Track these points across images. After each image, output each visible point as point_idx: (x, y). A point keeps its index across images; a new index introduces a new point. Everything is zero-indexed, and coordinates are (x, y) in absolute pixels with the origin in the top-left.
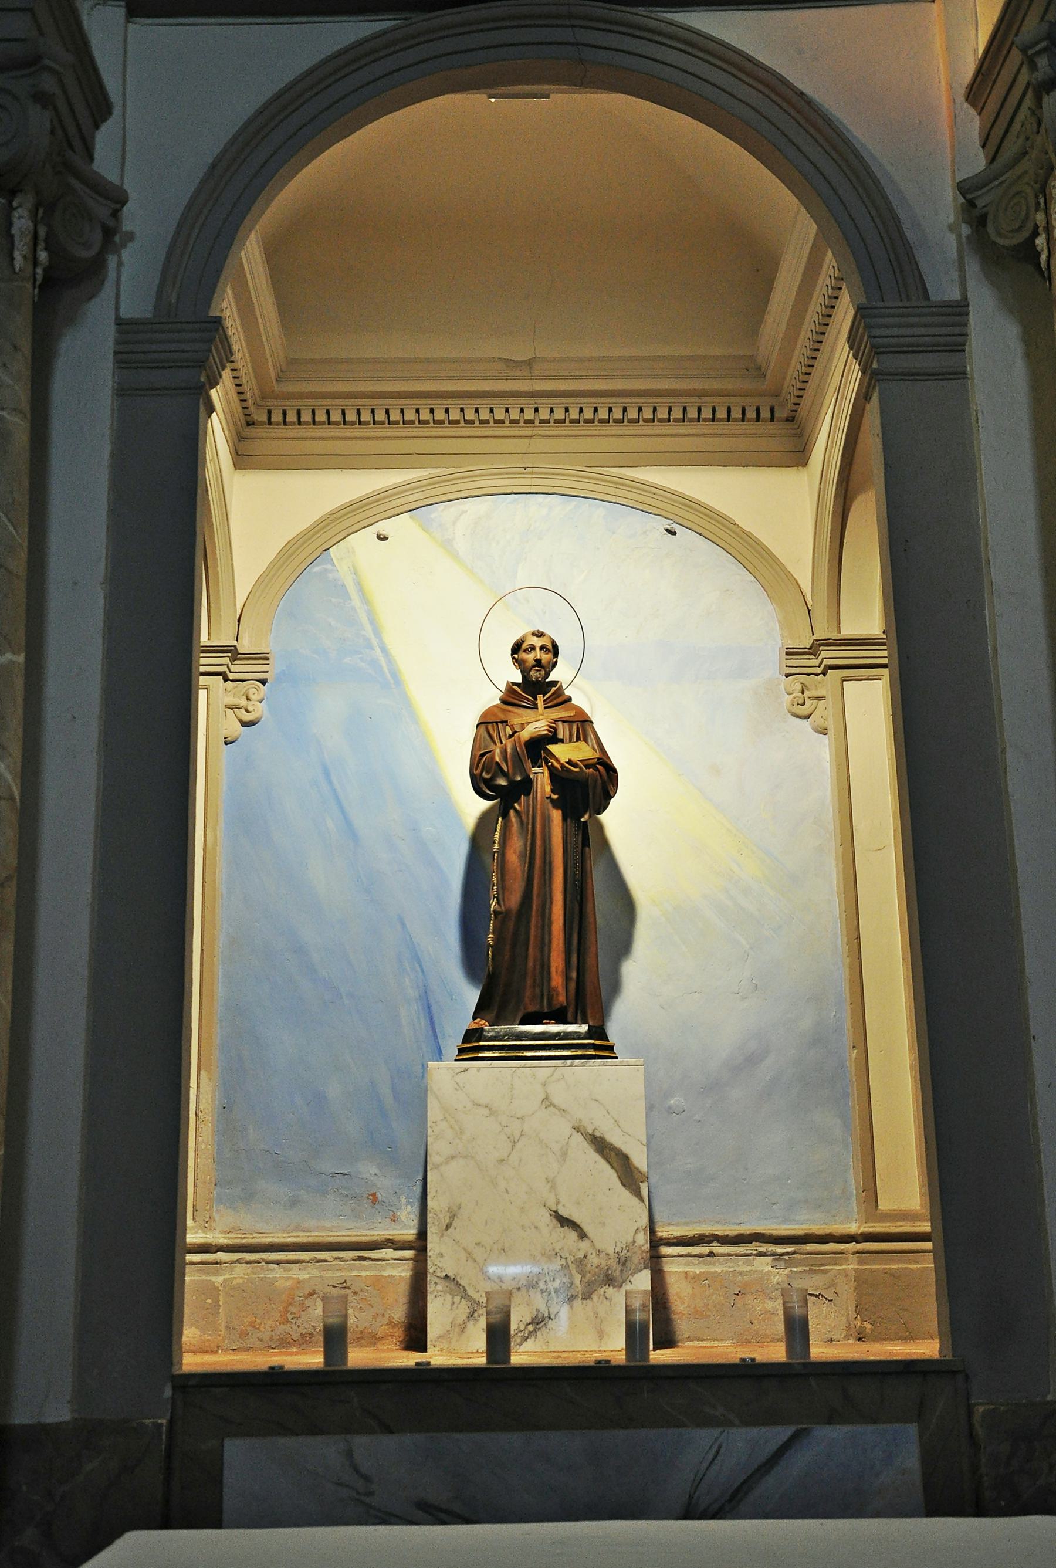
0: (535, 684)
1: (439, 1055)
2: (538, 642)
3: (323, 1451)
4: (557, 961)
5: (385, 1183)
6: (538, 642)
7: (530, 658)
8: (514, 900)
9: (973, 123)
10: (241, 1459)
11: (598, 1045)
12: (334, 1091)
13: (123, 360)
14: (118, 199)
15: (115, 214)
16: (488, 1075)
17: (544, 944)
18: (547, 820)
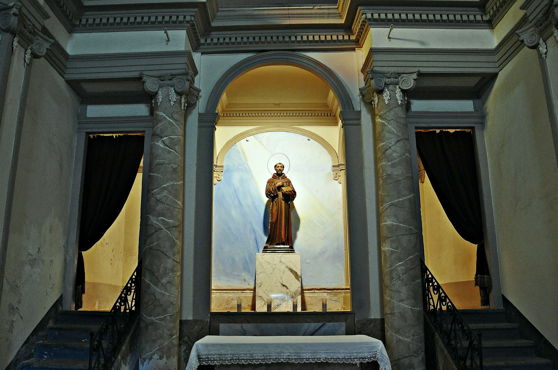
0: (279, 174)
1: (258, 251)
2: (280, 165)
3: (237, 326)
4: (283, 232)
5: (244, 275)
6: (280, 165)
7: (278, 169)
8: (274, 220)
9: (362, 76)
10: (222, 326)
11: (291, 250)
12: (237, 258)
13: (200, 121)
14: (199, 91)
15: (198, 94)
16: (269, 256)
17: (280, 229)
18: (281, 203)
